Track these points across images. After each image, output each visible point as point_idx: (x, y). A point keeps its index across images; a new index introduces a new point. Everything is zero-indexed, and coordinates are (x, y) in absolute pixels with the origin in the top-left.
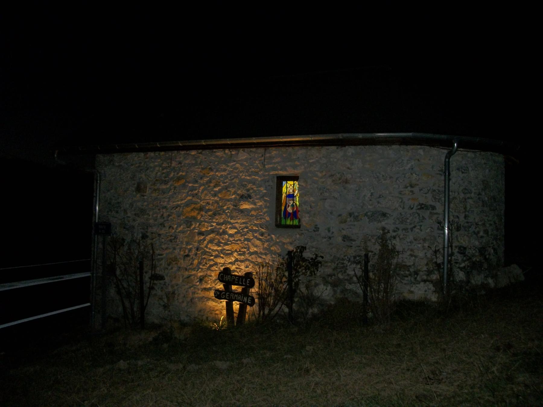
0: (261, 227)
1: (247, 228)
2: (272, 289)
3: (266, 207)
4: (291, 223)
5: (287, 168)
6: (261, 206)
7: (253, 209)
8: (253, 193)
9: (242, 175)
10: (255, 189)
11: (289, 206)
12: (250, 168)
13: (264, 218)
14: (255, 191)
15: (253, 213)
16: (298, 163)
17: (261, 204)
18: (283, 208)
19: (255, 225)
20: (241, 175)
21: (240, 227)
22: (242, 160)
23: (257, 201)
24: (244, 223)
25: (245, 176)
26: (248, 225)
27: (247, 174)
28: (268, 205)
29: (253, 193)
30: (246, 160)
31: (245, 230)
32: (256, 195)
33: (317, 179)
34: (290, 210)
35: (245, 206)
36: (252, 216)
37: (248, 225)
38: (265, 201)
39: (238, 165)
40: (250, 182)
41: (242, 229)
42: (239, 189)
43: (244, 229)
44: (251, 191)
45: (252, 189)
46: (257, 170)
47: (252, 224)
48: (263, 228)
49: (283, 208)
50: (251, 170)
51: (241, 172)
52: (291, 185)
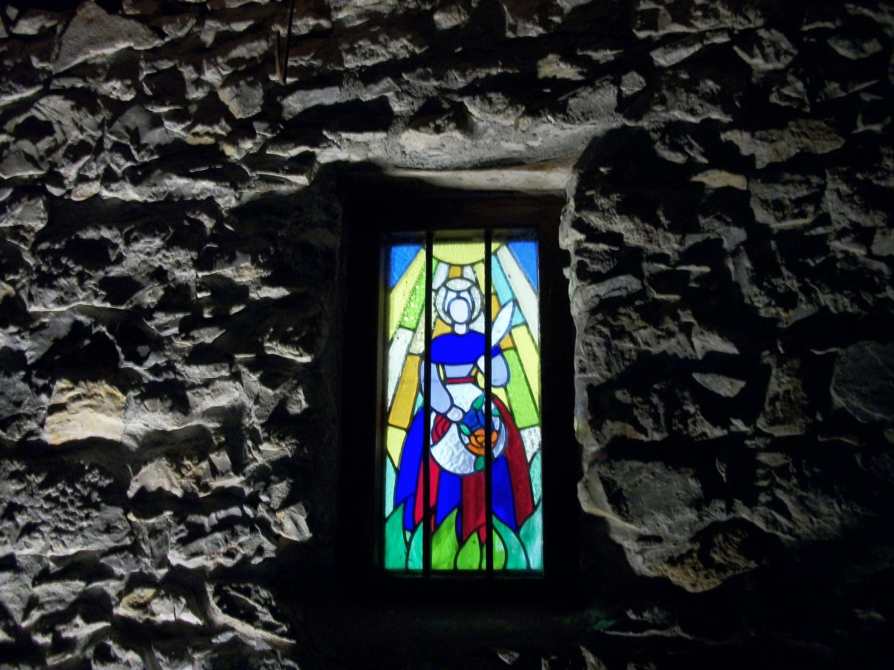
0: (232, 608)
1: (93, 606)
2: (90, 277)
3: (279, 422)
4: (471, 558)
5: (474, 110)
6: (231, 418)
7: (156, 445)
8: (164, 306)
9: (82, 179)
10: (188, 275)
11: (444, 422)
12: (156, 122)
13: (265, 526)
14: (176, 298)
15: (156, 476)
16: (568, 72)
17: (230, 394)
18: (395, 441)
19: (181, 584)
20: (71, 172)
21: (33, 603)
22: (86, 70)
23: (196, 373)
24: (71, 568)
25: (108, 178)
26: (111, 587)
27: (121, 164)
28: (299, 403)
29: (164, 306)
30: (123, 66)
31: (81, 630)
32: (186, 329)
33: (737, 182)
34: (450, 454)
35: (92, 417)
36: (151, 502)
37: (111, 587)
38: (273, 372)
39: (54, 108)
40: (136, 219)
41: (48, 624)
42: (46, 281)
43: (65, 617)
44: (149, 296)
45: (159, 275)
46: (202, 135)
47: (138, 580)
48: (250, 617)
49: (395, 441)
50: (154, 137)
51: (76, 152)
52: (457, 269)
